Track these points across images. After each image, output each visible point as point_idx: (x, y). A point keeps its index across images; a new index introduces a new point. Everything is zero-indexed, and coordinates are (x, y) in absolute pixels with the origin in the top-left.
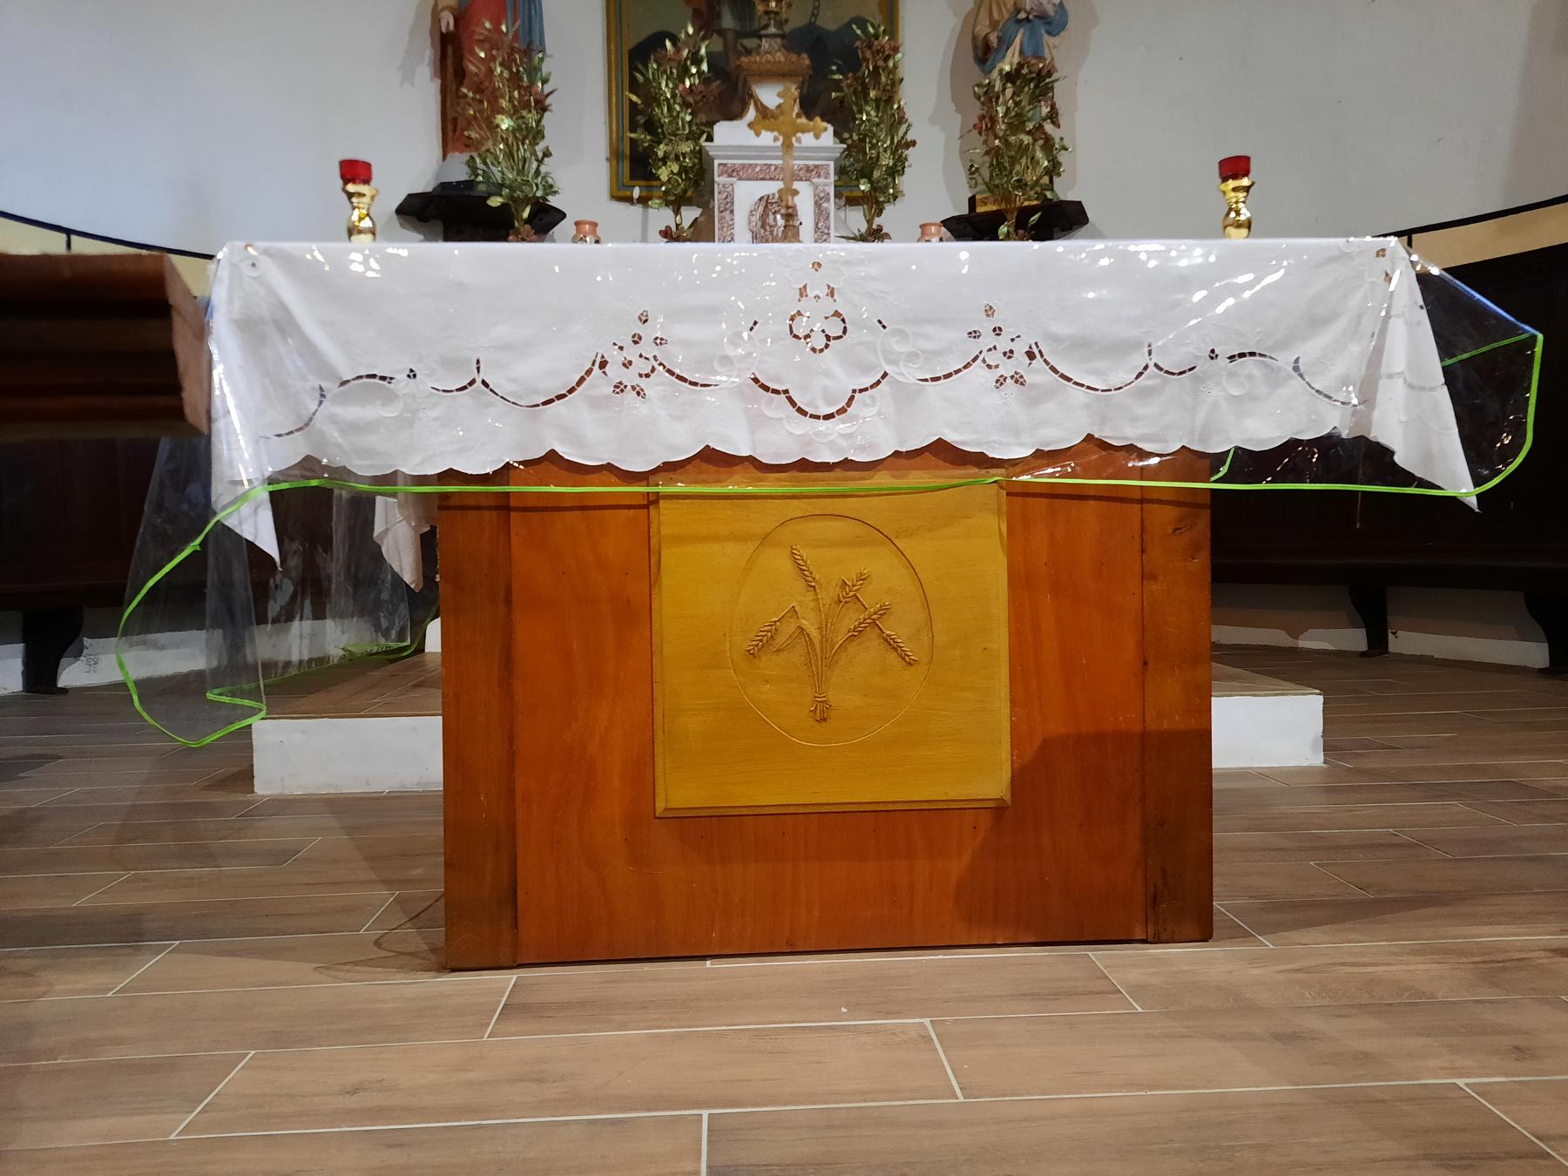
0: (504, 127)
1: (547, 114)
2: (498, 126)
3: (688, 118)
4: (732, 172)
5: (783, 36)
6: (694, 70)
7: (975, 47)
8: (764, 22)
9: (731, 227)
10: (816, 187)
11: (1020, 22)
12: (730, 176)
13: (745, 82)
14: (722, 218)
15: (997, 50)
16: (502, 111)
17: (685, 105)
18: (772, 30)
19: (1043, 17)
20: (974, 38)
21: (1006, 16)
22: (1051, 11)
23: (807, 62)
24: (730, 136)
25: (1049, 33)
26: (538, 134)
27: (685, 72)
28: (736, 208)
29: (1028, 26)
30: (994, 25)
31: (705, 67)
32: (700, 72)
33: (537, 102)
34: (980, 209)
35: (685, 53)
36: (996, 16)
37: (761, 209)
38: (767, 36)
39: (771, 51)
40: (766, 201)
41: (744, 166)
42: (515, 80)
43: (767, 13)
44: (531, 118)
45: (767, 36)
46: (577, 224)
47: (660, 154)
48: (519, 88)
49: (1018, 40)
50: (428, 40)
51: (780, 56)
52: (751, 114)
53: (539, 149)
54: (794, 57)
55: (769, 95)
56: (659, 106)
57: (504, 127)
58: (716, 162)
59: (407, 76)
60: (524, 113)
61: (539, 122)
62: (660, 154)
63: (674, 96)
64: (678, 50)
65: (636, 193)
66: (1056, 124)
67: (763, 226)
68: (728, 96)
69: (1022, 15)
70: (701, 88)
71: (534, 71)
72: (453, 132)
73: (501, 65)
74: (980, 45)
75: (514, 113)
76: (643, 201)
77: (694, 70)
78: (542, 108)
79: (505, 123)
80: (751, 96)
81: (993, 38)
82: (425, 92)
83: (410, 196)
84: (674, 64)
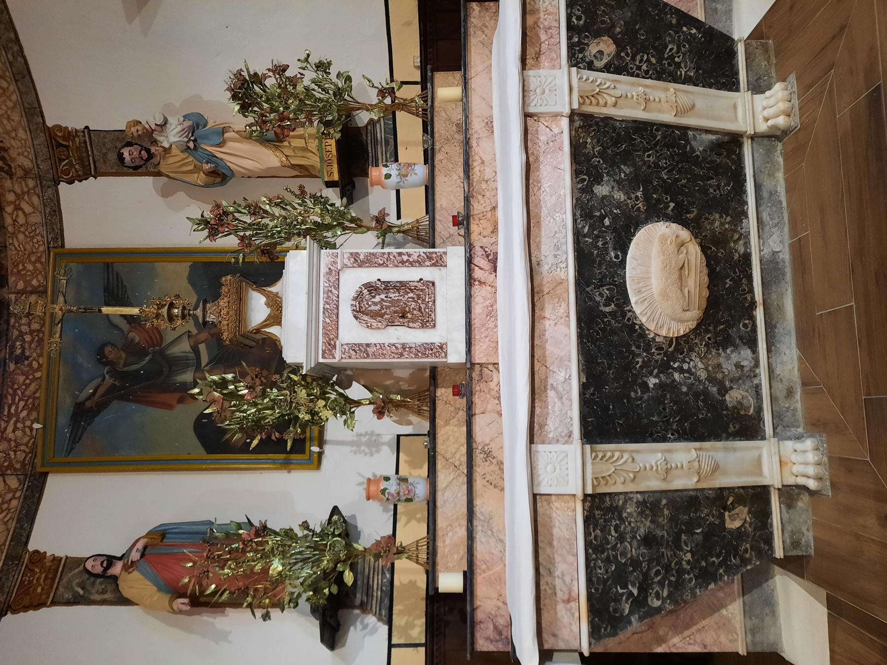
0: (280, 568)
1: (269, 526)
2: (280, 573)
3: (275, 390)
4: (331, 345)
5: (205, 302)
6: (232, 387)
7: (213, 185)
8: (191, 322)
9: (382, 346)
10: (345, 266)
11: (195, 147)
12: (335, 347)
13: (244, 336)
14: (375, 356)
15: (217, 165)
16: (265, 570)
17: (264, 395)
18: (199, 312)
19: (193, 129)
20: (206, 186)
21: (191, 159)
22: (188, 123)
23: (229, 277)
24: (296, 350)
25: (205, 126)
26: (289, 534)
27: (233, 395)
28: (364, 341)
29: (199, 141)
30: (197, 169)
31: (230, 376)
32: (235, 381)
33: (257, 535)
34: (336, 177)
35: (217, 394)
36: (191, 167)
37: (365, 318)
38: (204, 316)
39: (217, 313)
40: (359, 312)
41: (325, 334)
42: (237, 556)
43: (184, 317)
44: (271, 541)
45: (204, 316)
46: (368, 498)
47: (307, 417)
48: (244, 551)
49: (209, 149)
50: (196, 618)
51: (223, 302)
52: (273, 330)
53: (300, 533)
54: (224, 289)
55: (258, 308)
56: (264, 418)
57: (280, 568)
58: (321, 360)
59: (223, 636)
60: (267, 548)
61: (276, 533)
62: (307, 417)
63: (255, 405)
64: (214, 402)
65: (315, 449)
66: (285, 68)
67: (382, 316)
68: (260, 355)
69: (191, 145)
70: (249, 378)
71: (230, 537)
72: (256, 594)
73: (222, 568)
74: (211, 179)
75: (267, 556)
76: (321, 443)
77: (232, 387)
78: (264, 530)
79: (277, 566)
80: (258, 331)
81: (207, 167)
82: (238, 623)
83: (322, 641)
84: (226, 404)
